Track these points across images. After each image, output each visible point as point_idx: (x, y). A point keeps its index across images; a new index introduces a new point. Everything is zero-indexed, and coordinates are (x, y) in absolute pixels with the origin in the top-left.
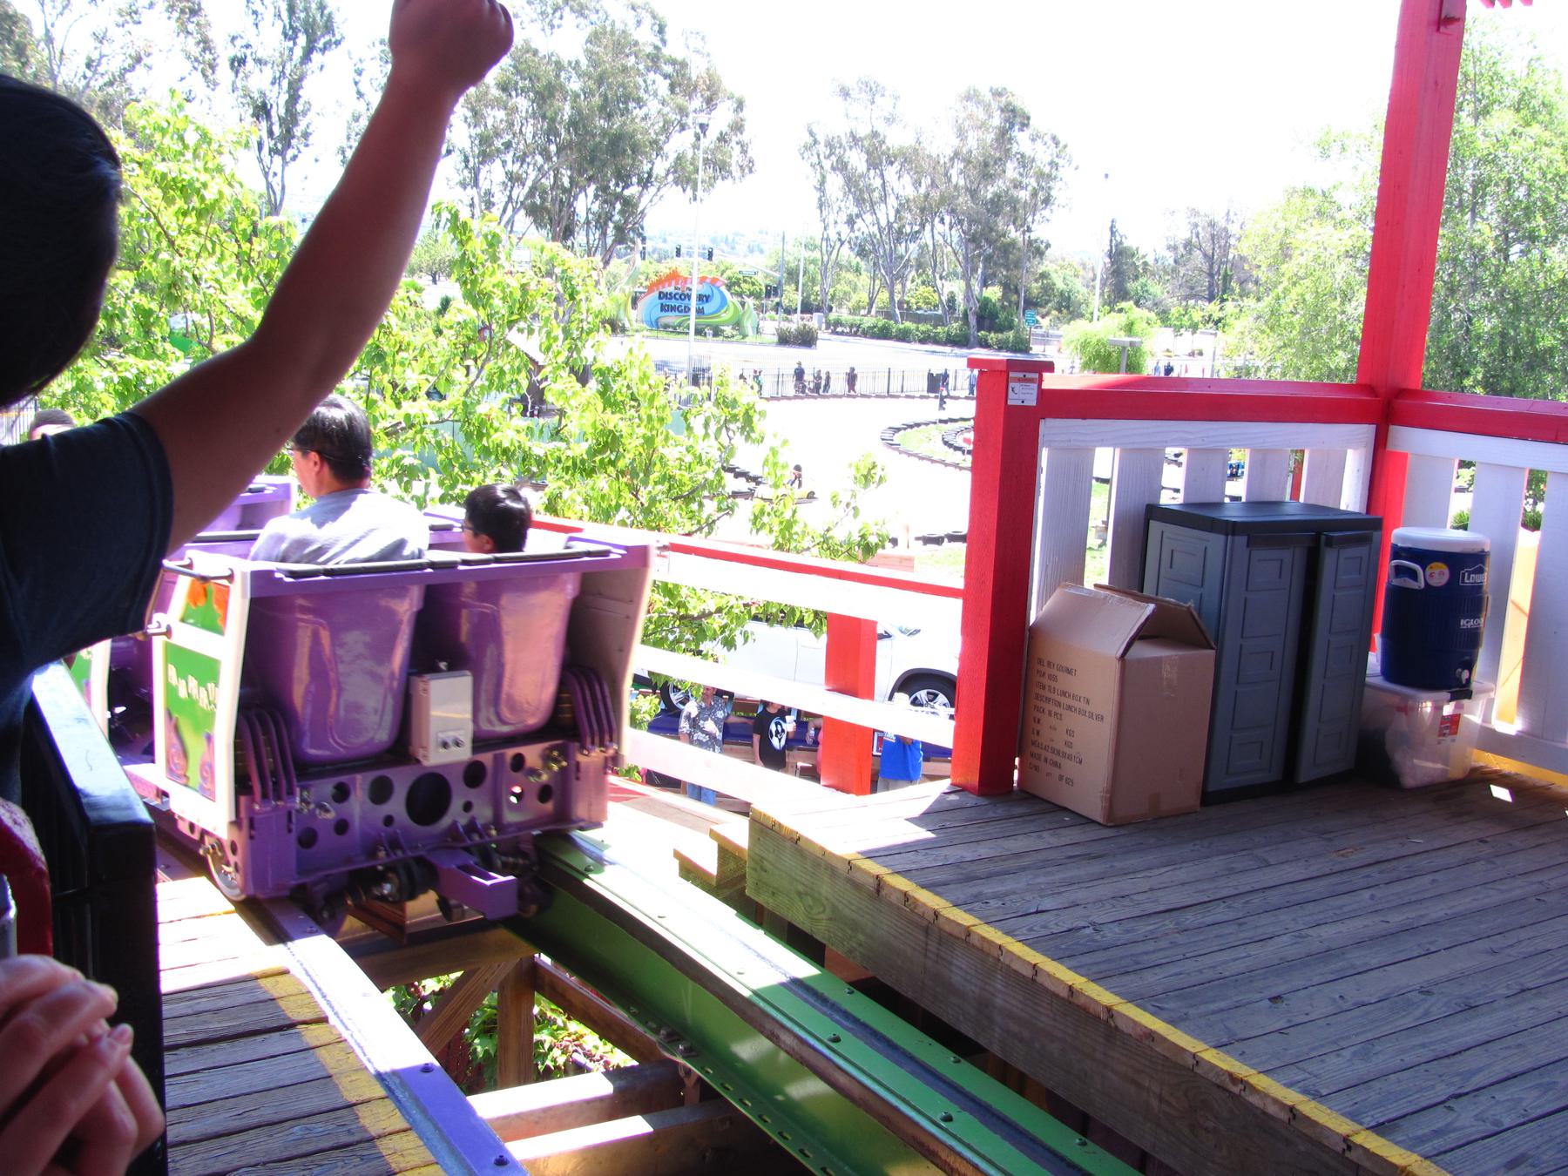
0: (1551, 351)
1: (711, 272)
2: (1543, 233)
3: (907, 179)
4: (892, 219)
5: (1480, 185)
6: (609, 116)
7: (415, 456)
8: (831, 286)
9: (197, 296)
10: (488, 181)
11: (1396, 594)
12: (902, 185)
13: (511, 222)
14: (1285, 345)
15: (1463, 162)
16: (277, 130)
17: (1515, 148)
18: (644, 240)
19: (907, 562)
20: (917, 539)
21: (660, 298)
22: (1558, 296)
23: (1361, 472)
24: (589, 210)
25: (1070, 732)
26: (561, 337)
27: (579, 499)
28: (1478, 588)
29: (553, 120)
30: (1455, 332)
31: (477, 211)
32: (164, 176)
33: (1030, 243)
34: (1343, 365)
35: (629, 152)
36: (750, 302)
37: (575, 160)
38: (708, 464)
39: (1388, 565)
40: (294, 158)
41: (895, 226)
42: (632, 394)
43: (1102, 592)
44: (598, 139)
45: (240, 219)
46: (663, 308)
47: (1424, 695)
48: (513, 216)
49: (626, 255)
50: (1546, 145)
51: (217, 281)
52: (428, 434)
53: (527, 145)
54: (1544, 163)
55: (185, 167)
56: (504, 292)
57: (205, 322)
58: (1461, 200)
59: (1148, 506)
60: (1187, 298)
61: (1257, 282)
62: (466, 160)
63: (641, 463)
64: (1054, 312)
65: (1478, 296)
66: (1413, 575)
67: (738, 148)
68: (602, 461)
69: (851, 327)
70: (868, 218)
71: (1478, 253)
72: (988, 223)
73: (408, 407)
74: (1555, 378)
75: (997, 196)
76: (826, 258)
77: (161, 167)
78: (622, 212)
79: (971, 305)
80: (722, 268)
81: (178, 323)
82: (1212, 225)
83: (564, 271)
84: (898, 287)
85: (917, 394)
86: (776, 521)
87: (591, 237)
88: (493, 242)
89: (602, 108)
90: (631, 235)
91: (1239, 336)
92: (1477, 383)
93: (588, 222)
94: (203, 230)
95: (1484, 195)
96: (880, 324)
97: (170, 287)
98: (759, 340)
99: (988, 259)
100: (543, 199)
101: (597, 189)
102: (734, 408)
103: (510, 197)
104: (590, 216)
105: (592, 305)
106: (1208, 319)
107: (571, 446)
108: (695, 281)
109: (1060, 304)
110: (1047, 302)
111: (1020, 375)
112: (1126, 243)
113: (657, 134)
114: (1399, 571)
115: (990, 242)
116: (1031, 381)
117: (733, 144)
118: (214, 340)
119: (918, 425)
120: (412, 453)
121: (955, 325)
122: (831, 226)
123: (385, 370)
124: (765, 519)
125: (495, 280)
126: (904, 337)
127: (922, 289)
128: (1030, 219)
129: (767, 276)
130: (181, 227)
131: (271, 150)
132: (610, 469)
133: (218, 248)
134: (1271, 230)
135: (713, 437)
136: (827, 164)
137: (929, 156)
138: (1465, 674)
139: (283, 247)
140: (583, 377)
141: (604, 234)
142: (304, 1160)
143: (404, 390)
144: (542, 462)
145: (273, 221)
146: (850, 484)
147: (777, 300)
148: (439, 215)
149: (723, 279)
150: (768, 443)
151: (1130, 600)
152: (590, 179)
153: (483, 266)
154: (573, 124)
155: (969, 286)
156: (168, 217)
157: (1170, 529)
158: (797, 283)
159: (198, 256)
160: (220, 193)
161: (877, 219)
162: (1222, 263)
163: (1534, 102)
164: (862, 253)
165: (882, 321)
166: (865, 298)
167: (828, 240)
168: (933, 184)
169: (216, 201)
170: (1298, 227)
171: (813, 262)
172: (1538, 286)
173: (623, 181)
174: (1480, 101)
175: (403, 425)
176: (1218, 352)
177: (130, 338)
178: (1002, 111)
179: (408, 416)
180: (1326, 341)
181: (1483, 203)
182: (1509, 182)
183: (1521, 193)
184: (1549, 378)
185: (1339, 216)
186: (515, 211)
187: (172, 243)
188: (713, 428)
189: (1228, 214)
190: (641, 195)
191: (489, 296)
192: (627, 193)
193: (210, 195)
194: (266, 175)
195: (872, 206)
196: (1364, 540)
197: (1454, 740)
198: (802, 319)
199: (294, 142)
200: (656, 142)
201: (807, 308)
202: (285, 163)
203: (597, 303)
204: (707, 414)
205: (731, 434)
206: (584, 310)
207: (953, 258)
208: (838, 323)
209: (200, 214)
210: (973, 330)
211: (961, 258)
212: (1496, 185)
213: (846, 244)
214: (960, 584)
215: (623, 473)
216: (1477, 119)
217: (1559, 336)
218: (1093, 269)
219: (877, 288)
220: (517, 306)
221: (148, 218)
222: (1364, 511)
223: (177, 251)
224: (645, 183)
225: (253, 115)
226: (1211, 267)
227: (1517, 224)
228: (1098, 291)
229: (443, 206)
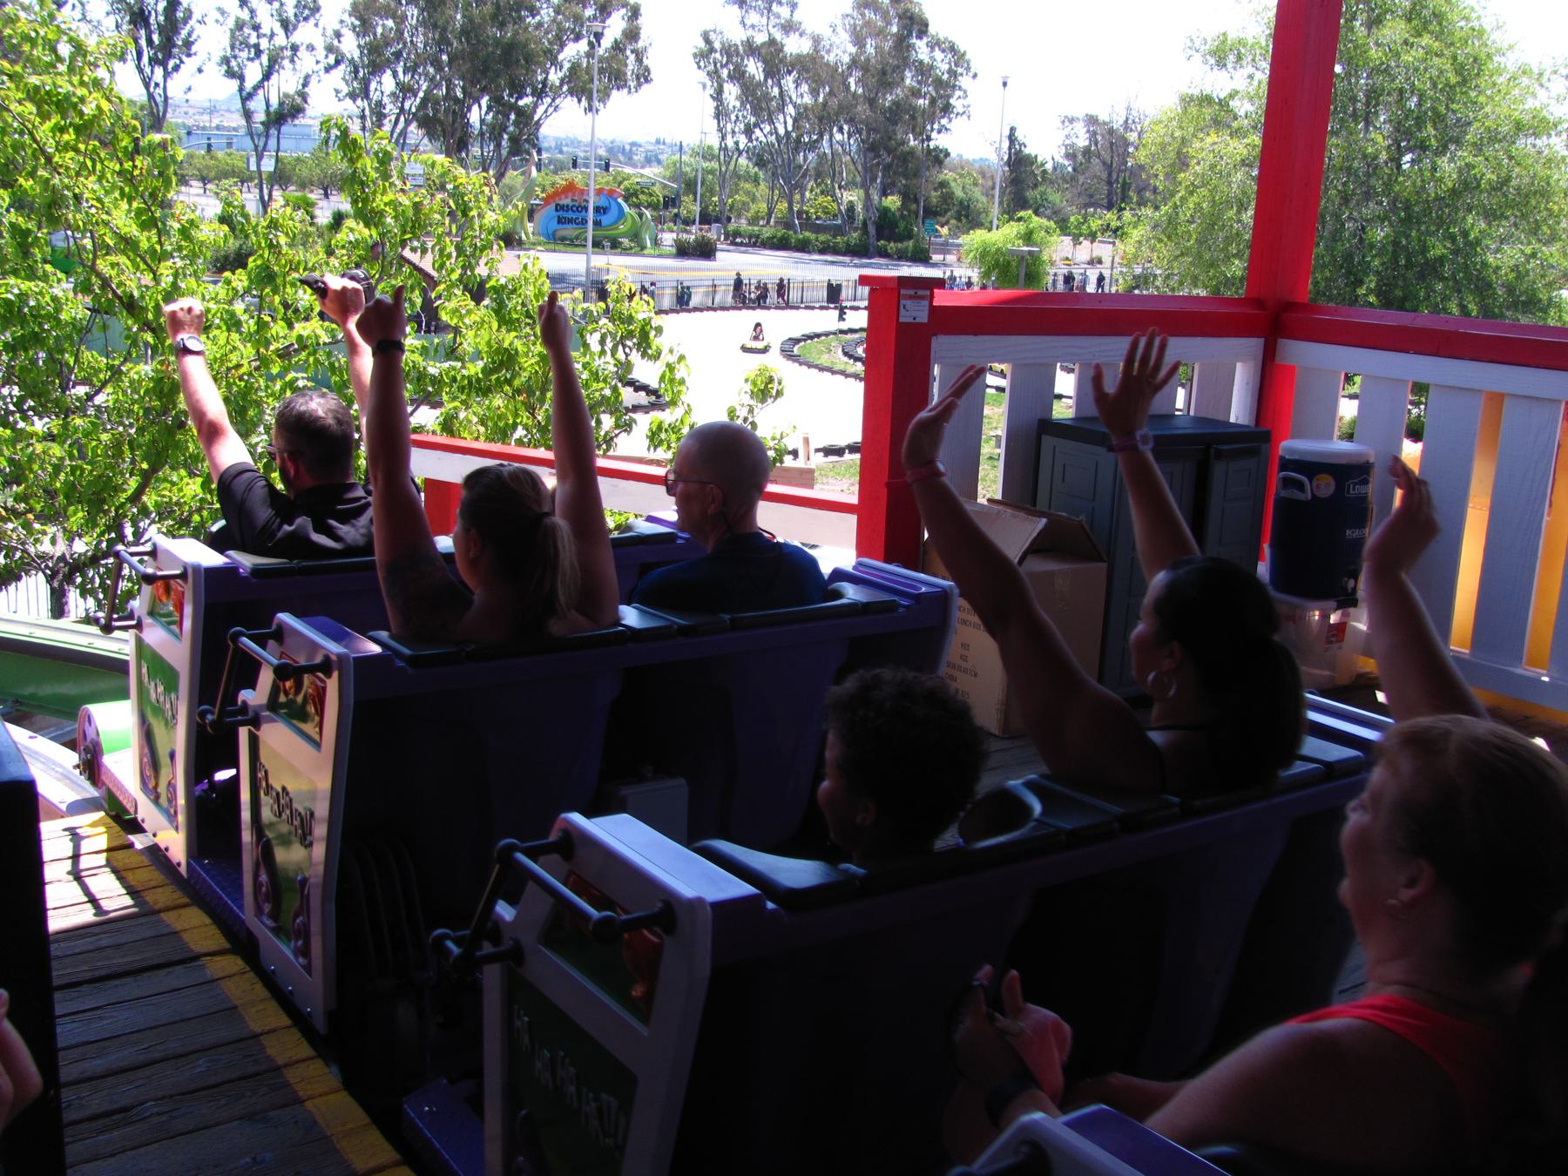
0: (1441, 260)
1: (607, 183)
2: (1433, 142)
3: (805, 88)
4: (790, 128)
5: (1373, 95)
6: (502, 25)
7: (308, 379)
8: (729, 197)
9: (78, 216)
10: (378, 93)
11: (1284, 506)
12: (799, 93)
13: (404, 133)
14: (1182, 254)
15: (1356, 71)
16: (156, 38)
17: (1407, 58)
18: (539, 152)
19: (806, 477)
20: (818, 450)
21: (557, 210)
22: (1448, 206)
23: (1251, 384)
24: (482, 121)
25: (965, 646)
26: (454, 254)
27: (475, 419)
28: (1363, 499)
29: (444, 29)
30: (1349, 241)
31: (368, 124)
32: (37, 89)
33: (929, 151)
34: (1239, 273)
35: (523, 62)
36: (648, 213)
37: (468, 71)
38: (605, 381)
39: (1277, 476)
40: (177, 68)
41: (794, 135)
42: (527, 311)
43: (996, 507)
44: (490, 49)
45: (121, 135)
46: (560, 221)
47: (1310, 604)
48: (405, 129)
49: (521, 167)
50: (1436, 55)
51: (99, 200)
52: (321, 356)
53: (417, 55)
54: (1435, 73)
55: (59, 81)
56: (395, 210)
57: (88, 243)
58: (1354, 110)
59: (1040, 420)
60: (1087, 206)
61: (1155, 190)
62: (356, 72)
63: (537, 382)
64: (953, 222)
65: (1371, 205)
66: (1300, 486)
67: (632, 57)
68: (498, 379)
69: (750, 238)
70: (767, 128)
71: (1371, 161)
72: (887, 131)
73: (301, 328)
74: (1446, 287)
75: (896, 104)
76: (723, 169)
77: (34, 80)
78: (516, 123)
79: (871, 214)
80: (620, 179)
81: (59, 240)
82: (1111, 132)
83: (456, 188)
84: (797, 197)
85: (817, 305)
86: (673, 437)
87: (486, 150)
88: (384, 160)
89: (494, 17)
90: (527, 146)
91: (1136, 245)
92: (1370, 291)
93: (482, 134)
94: (82, 147)
95: (1377, 104)
96: (779, 234)
97: (50, 207)
98: (657, 252)
99: (887, 168)
100: (436, 111)
101: (490, 100)
102: (629, 324)
103: (402, 109)
104: (484, 127)
105: (485, 221)
106: (1106, 228)
107: (468, 365)
108: (592, 194)
109: (959, 212)
110: (946, 212)
111: (912, 292)
112: (1026, 151)
113: (550, 43)
114: (1287, 482)
115: (889, 152)
116: (922, 298)
117: (628, 53)
118: (98, 262)
119: (818, 336)
120: (305, 375)
121: (855, 235)
122: (729, 137)
123: (275, 291)
124: (663, 436)
125: (386, 199)
126: (803, 247)
127: (820, 199)
128: (929, 127)
129: (665, 186)
130: (58, 143)
131: (150, 59)
132: (507, 388)
133: (99, 167)
134: (1167, 139)
135: (609, 353)
136: (725, 73)
137: (827, 64)
138: (1351, 583)
139: (168, 166)
140: (478, 292)
141: (498, 146)
142: (212, 1091)
143: (296, 311)
144: (437, 381)
145: (157, 137)
146: (747, 400)
147: (676, 210)
148: (328, 132)
149: (620, 190)
150: (666, 358)
151: (1022, 514)
152: (483, 90)
153: (374, 184)
154: (464, 32)
155: (868, 196)
156: (44, 131)
157: (1067, 446)
158: (695, 194)
159: (78, 174)
160: (99, 108)
161: (775, 128)
162: (1120, 171)
163: (1425, 12)
164: (760, 163)
165: (781, 232)
166: (763, 207)
167: (726, 149)
168: (831, 93)
169: (94, 116)
170: (1194, 136)
171: (712, 172)
172: (1429, 195)
173: (517, 92)
174: (1373, 10)
175: (296, 346)
176: (1117, 259)
177: (9, 260)
178: (900, 18)
179: (300, 337)
180: (1222, 250)
181: (1376, 113)
182: (1401, 92)
183: (1412, 103)
184: (1439, 286)
185: (1235, 124)
186: (408, 123)
187: (49, 159)
188: (609, 344)
189: (1126, 121)
190: (536, 106)
191: (381, 214)
192: (521, 103)
193: (89, 110)
194: (147, 86)
195: (770, 116)
196: (1254, 452)
197: (1340, 648)
198: (701, 230)
199: (175, 50)
200: (550, 51)
201: (706, 219)
202: (167, 75)
203: (490, 218)
204: (603, 331)
205: (627, 350)
206: (477, 227)
207: (852, 168)
208: (737, 234)
209: (78, 130)
210: (872, 240)
211: (860, 168)
212: (1389, 94)
213: (744, 154)
214: (854, 500)
215: (518, 391)
216: (1369, 28)
217: (1449, 245)
218: (992, 177)
219: (775, 198)
220: (410, 224)
221: (22, 133)
222: (1253, 424)
223: (55, 169)
224: (539, 94)
225: (130, 22)
226: (1110, 175)
227: (1408, 134)
228: (997, 200)
229: (332, 122)
